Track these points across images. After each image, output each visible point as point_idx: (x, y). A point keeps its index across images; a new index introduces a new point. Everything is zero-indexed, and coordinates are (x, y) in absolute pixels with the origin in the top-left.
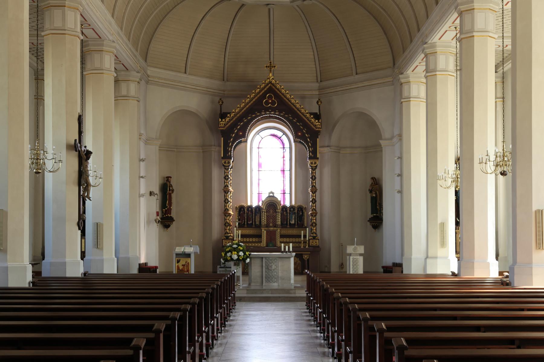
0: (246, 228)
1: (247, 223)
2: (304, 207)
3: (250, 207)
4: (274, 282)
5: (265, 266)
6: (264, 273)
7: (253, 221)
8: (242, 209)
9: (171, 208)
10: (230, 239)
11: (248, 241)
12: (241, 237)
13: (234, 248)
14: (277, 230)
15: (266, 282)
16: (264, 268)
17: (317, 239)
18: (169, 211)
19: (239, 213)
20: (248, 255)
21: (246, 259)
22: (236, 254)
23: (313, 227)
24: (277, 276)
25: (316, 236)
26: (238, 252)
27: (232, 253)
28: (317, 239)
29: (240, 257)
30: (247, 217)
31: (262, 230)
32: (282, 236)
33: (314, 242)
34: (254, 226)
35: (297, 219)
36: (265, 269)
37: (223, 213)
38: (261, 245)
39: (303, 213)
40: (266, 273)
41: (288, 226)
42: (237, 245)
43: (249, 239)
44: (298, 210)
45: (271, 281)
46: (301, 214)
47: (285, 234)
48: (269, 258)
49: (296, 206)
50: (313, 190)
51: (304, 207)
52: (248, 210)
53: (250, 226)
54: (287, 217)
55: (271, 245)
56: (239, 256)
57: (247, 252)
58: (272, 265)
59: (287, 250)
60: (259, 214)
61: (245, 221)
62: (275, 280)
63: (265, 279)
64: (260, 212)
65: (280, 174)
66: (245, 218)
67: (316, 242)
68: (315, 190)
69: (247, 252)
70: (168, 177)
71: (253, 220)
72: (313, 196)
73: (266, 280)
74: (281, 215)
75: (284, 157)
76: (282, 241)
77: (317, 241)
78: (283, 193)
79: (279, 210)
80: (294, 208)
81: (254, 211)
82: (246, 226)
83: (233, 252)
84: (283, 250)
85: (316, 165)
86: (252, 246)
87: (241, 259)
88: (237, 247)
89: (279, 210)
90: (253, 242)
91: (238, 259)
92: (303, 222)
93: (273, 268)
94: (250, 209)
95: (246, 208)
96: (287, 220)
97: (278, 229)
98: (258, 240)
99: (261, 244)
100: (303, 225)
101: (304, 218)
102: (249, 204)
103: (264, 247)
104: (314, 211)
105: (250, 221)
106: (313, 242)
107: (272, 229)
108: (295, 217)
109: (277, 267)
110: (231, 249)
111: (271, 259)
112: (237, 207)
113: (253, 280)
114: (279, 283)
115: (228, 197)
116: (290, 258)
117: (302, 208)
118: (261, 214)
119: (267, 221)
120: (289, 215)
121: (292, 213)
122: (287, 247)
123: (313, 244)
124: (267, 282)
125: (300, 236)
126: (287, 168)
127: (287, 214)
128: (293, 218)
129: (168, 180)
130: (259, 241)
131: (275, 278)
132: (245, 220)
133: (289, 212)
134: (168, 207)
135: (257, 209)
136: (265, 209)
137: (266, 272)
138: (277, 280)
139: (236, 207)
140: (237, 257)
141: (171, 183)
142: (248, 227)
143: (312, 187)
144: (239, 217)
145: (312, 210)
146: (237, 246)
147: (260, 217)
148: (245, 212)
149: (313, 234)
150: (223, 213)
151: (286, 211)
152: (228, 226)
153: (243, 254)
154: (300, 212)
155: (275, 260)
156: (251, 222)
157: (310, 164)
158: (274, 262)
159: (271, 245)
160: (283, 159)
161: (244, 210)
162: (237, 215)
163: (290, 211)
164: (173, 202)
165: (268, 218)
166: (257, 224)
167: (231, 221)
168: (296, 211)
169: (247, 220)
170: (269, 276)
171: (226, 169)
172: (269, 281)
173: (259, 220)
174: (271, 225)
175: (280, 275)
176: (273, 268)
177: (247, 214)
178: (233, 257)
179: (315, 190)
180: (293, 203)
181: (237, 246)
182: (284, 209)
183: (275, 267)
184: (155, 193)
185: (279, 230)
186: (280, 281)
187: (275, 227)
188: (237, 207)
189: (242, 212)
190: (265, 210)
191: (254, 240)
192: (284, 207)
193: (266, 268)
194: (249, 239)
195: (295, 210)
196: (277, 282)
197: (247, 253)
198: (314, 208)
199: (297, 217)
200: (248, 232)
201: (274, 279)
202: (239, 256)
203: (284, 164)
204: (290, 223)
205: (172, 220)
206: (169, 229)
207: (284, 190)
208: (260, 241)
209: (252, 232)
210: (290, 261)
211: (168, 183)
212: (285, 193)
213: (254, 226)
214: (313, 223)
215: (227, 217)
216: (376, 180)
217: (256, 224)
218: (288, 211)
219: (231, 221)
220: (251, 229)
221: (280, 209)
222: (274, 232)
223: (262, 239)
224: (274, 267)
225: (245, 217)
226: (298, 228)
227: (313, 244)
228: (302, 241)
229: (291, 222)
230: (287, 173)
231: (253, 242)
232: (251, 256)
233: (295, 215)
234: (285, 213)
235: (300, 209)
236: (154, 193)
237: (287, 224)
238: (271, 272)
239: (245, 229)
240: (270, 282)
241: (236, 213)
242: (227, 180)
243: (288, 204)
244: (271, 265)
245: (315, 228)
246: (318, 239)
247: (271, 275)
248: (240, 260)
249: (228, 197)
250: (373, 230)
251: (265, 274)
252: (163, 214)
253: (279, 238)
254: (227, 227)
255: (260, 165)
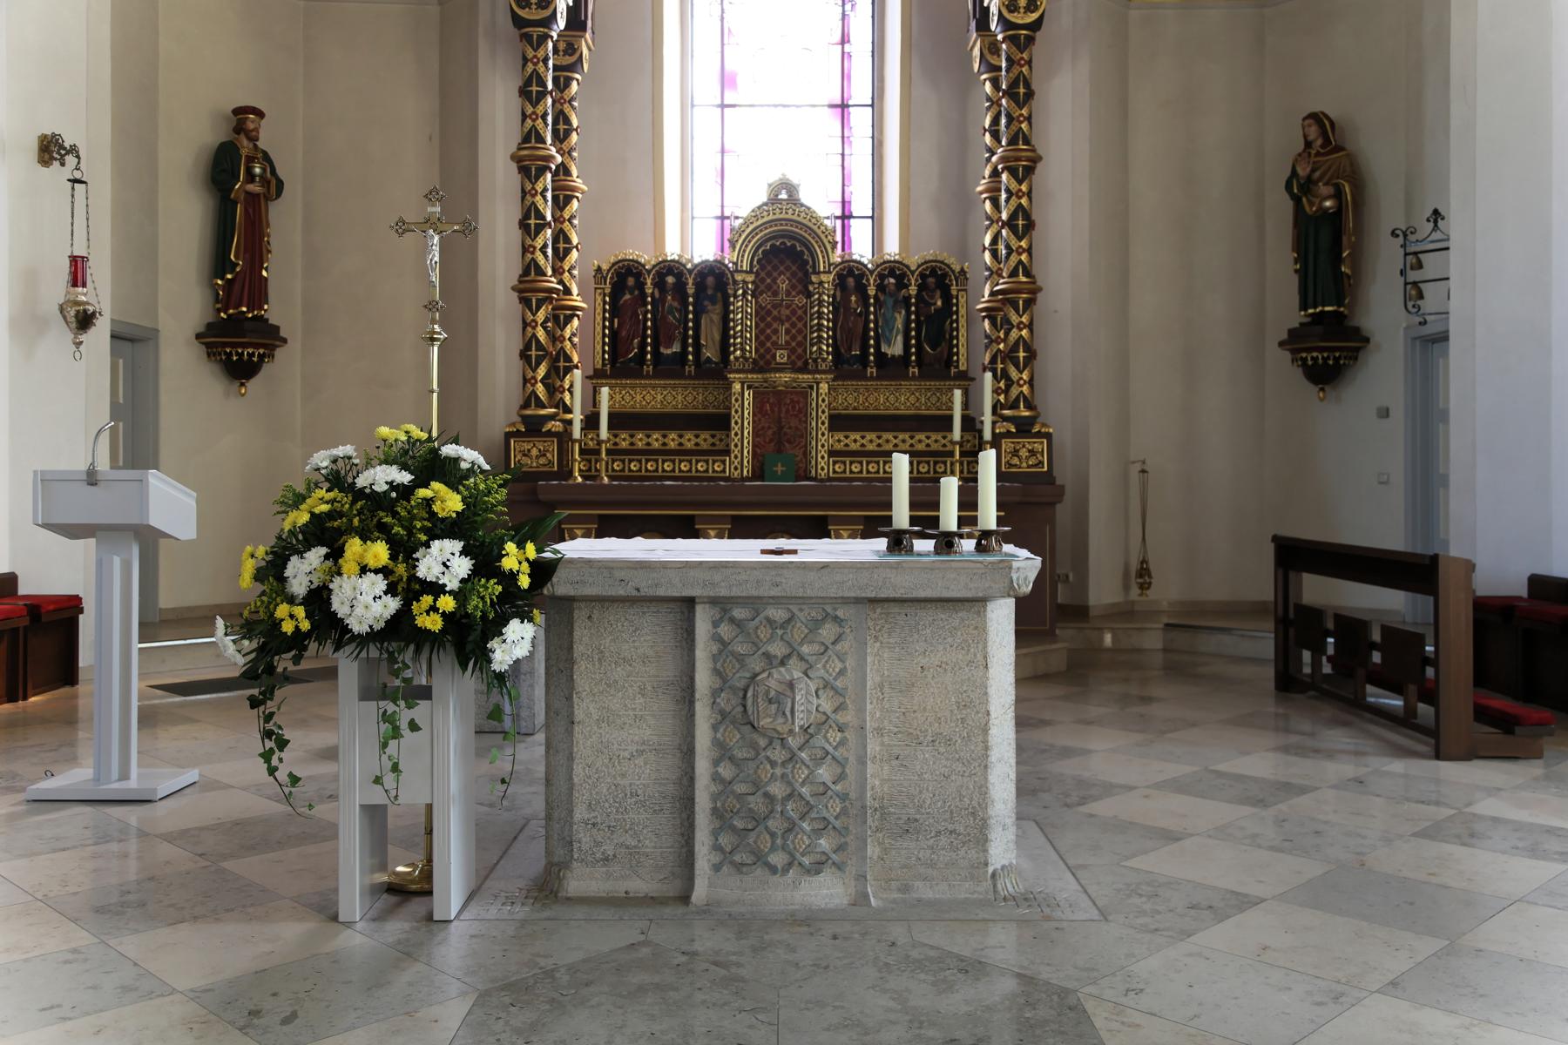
0: (648, 377)
1: (656, 353)
2: (957, 269)
3: (670, 269)
4: (817, 868)
5: (715, 693)
6: (702, 767)
7: (684, 345)
8: (631, 281)
9: (264, 273)
10: (550, 433)
11: (656, 445)
12: (610, 428)
13: (375, 501)
14: (811, 388)
15: (726, 860)
16: (702, 712)
17: (1039, 435)
18: (258, 292)
19: (614, 303)
20: (524, 582)
21: (495, 627)
22: (385, 571)
23: (1017, 366)
24: (844, 797)
25: (1031, 421)
26: (404, 550)
27: (336, 554)
28: (1039, 435)
29: (427, 600)
30: (654, 320)
31: (729, 387)
32: (838, 422)
33: (1024, 453)
34: (690, 369)
35: (918, 330)
36: (715, 728)
37: (513, 288)
38: (724, 471)
39: (947, 297)
40: (726, 771)
41: (872, 371)
42: (404, 467)
43: (665, 436)
44: (922, 287)
45: (777, 859)
46: (939, 303)
47: (850, 412)
48: (755, 603)
49: (913, 261)
50: (1018, 159)
51: (957, 269)
52: (660, 283)
53: (669, 368)
54: (867, 321)
55: (779, 468)
56: (410, 588)
57: (510, 547)
58: (791, 685)
59: (949, 517)
60: (718, 308)
61: (643, 345)
62: (824, 843)
63: (715, 833)
64: (726, 297)
65: (832, 121)
66: (645, 328)
67: (1032, 453)
68: (1028, 160)
69: (510, 547)
70: (240, 112)
71: (686, 337)
72: (1019, 194)
73: (725, 840)
74: (836, 312)
75: (844, 40)
76: (838, 447)
77: (1038, 447)
78: (839, 213)
79: (824, 278)
80: (904, 275)
81: (691, 290)
82: (648, 369)
83: (354, 546)
84: (901, 515)
85: (1034, 16)
86: (677, 473)
87: (433, 623)
88: (405, 492)
89: (824, 278)
90: (682, 452)
91: (399, 628)
92: (951, 346)
93: (800, 720)
94: (670, 279)
95: (649, 272)
96: (865, 338)
97: (818, 384)
98: (711, 440)
99: (724, 462)
100: (948, 363)
101: (952, 330)
102: (672, 250)
103: (743, 479)
104: (1024, 279)
105: (669, 346)
106: (1015, 453)
107: (786, 377)
108: (907, 322)
109: (840, 708)
110: (330, 515)
111: (778, 614)
112: (605, 267)
113: (584, 838)
114: (861, 877)
115: (539, 198)
116: (978, 603)
117: (945, 275)
118: (726, 304)
119: (760, 344)
120: (875, 314)
121: (890, 302)
122: (950, 487)
123: (1015, 461)
124: (739, 867)
125: (945, 423)
126: (861, 91)
127: (867, 306)
128: (899, 324)
129: (239, 129)
130: (713, 444)
131: (824, 826)
132: (645, 337)
133: (876, 298)
134: (238, 269)
135: (710, 280)
136: (746, 272)
137: (723, 752)
138: (840, 848)
139: (599, 269)
140: (393, 604)
141: (260, 144)
142: (658, 375)
143: (1013, 141)
144: (612, 323)
145: (1014, 274)
146: (405, 478)
147: (725, 320)
148: (643, 295)
149: (1014, 406)
150: (513, 288)
151: (861, 290)
152: (538, 364)
153: (463, 566)
154: (932, 297)
155: (828, 632)
156: (676, 348)
157: (986, 52)
158: (805, 649)
159: (779, 468)
160: (840, 46)
161: (640, 286)
162: (604, 311)
163: (881, 288)
164: (274, 246)
165: (769, 325)
166: (709, 360)
167: (574, 345)
168: (913, 290)
169: (655, 337)
170: (757, 803)
171: (526, 38)
172: (759, 858)
173: (717, 337)
174: (781, 356)
175: (877, 778)
176: (800, 720)
177: (652, 303)
178: (339, 606)
179: (1028, 160)
180: (892, 248)
181: (405, 478)
182: (851, 281)
183: (827, 706)
184: (67, 145)
185: (824, 387)
186: (872, 850)
187: (804, 369)
188: (605, 267)
189: (627, 296)
190: (750, 278)
191: (690, 440)
192: (851, 274)
193: (722, 718)
194: (665, 436)
195: (907, 286)
196: (839, 867)
197: (513, 558)
198: (1020, 262)
199: (918, 321)
200: (659, 397)
201: (818, 833)
202: (410, 588)
203: (845, 76)
204: (880, 356)
205: (271, 338)
206: (254, 384)
207: (846, 200)
208: (721, 446)
209: (680, 398)
210: (982, 630)
211: (245, 146)
212: (851, 217)
213: (690, 369)
214: (1017, 343)
215: (534, 315)
216: (1332, 124)
217: (703, 358)
218: (872, 291)
219: (574, 345)
220: (674, 387)
221: (830, 272)
222: (798, 400)
223: (728, 436)
224: (807, 703)
225: (646, 320)
226: (923, 376)
227: (1015, 461)
228: (953, 443)
229: (884, 348)
230: (861, 120)
231: (682, 452)
232: (560, 585)
233: (908, 313)
234: (853, 298)
235: (931, 280)
236: (62, 147)
237: (863, 359)
238: (778, 754)
239: (644, 387)
240: (773, 870)
241: (599, 299)
242: (535, 105)
243: (861, 249)
244: (774, 681)
245: (1025, 376)
246: (1048, 436)
247: (777, 789)
248: (427, 632)
249: (539, 198)
250: (1312, 389)
251: (716, 778)
252: (219, 306)
253: (824, 428)
254: (534, 370)
255: (726, 80)
